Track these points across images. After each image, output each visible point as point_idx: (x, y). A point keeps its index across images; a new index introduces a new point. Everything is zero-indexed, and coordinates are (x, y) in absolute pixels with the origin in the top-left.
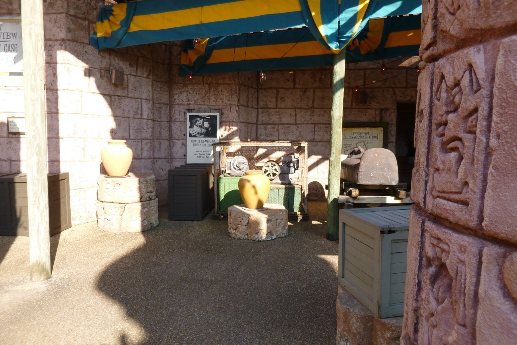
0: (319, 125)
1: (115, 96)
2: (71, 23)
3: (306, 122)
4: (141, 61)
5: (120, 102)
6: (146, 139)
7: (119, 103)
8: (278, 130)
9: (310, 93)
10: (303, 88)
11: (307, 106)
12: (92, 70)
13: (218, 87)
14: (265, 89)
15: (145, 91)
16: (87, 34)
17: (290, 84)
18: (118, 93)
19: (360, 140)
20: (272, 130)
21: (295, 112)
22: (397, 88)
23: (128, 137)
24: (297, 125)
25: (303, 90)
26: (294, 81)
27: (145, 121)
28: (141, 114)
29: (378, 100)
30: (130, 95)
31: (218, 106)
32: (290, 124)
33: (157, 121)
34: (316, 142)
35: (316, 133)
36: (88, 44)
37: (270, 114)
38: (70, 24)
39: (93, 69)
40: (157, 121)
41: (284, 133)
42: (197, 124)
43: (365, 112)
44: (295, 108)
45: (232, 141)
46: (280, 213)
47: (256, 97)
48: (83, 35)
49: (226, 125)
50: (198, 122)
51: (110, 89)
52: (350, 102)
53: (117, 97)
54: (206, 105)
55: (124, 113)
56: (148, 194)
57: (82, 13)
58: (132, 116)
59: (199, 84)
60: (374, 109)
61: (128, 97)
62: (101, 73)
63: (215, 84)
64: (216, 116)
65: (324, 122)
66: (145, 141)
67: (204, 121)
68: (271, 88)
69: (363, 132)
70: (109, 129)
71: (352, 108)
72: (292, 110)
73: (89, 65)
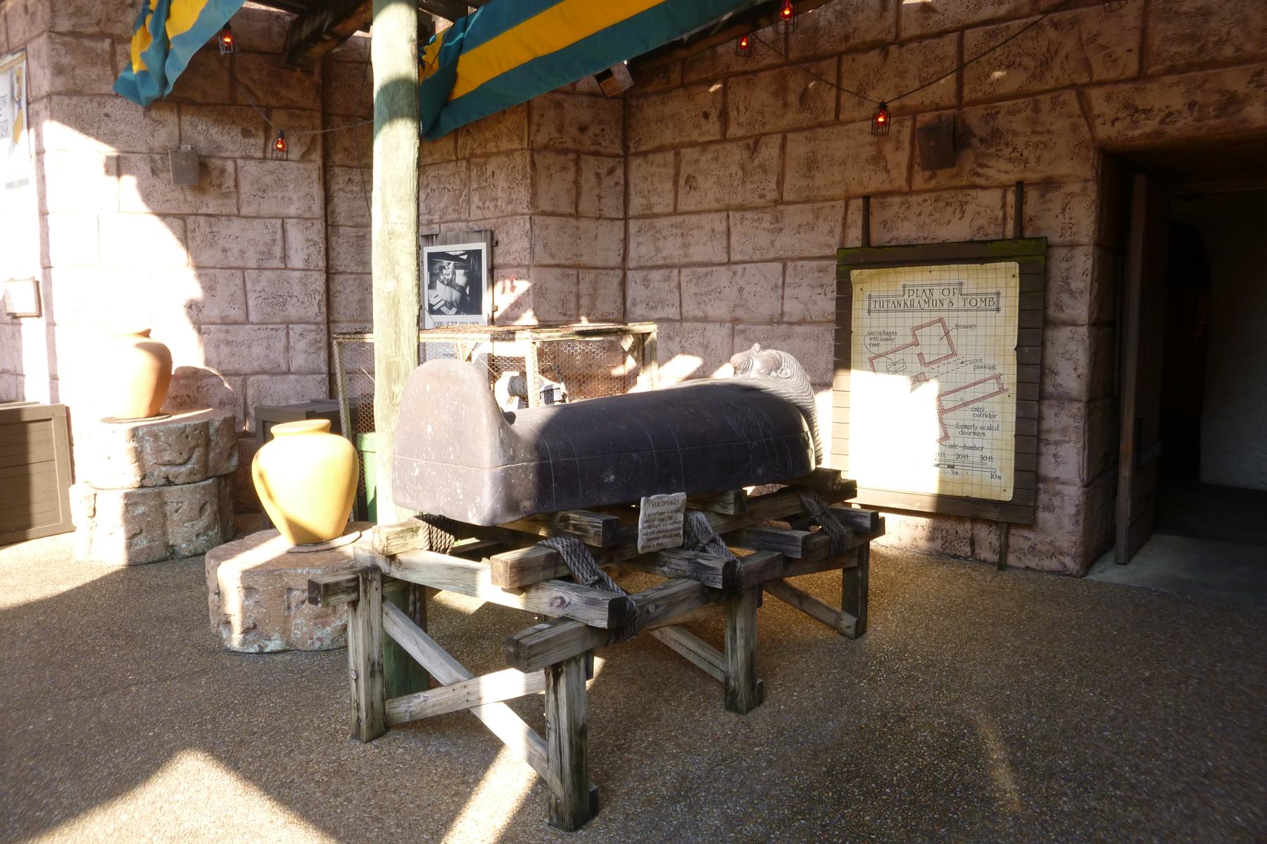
0: (800, 263)
1: (198, 217)
2: (63, 52)
3: (757, 256)
4: (279, 118)
5: (215, 229)
6: (301, 321)
7: (212, 232)
8: (679, 286)
9: (769, 152)
10: (750, 137)
11: (762, 196)
12: (126, 158)
13: (485, 164)
14: (645, 154)
15: (295, 197)
16: (109, 73)
17: (712, 129)
18: (208, 207)
19: (927, 317)
20: (663, 285)
21: (724, 223)
22: (1102, 83)
23: (243, 319)
24: (735, 267)
25: (751, 141)
26: (724, 117)
27: (297, 274)
28: (285, 258)
29: (1014, 149)
30: (244, 211)
31: (487, 222)
32: (712, 264)
33: (352, 273)
34: (791, 324)
35: (788, 291)
36: (112, 95)
37: (658, 236)
38: (59, 56)
39: (127, 155)
40: (352, 273)
41: (696, 294)
42: (442, 277)
43: (962, 204)
44: (727, 209)
45: (517, 323)
46: (299, 571)
47: (617, 184)
48: (98, 76)
49: (504, 277)
50: (444, 271)
51: (182, 199)
52: (904, 169)
53: (202, 220)
54: (462, 221)
55: (227, 258)
56: (163, 469)
57: (92, 22)
58: (252, 263)
59: (450, 161)
60: (998, 187)
61: (239, 216)
62: (153, 161)
63: (480, 156)
64: (479, 252)
65: (816, 252)
66: (298, 328)
67: (456, 267)
68: (660, 149)
69: (940, 285)
70: (183, 301)
71: (911, 192)
72: (716, 216)
73: (117, 148)
